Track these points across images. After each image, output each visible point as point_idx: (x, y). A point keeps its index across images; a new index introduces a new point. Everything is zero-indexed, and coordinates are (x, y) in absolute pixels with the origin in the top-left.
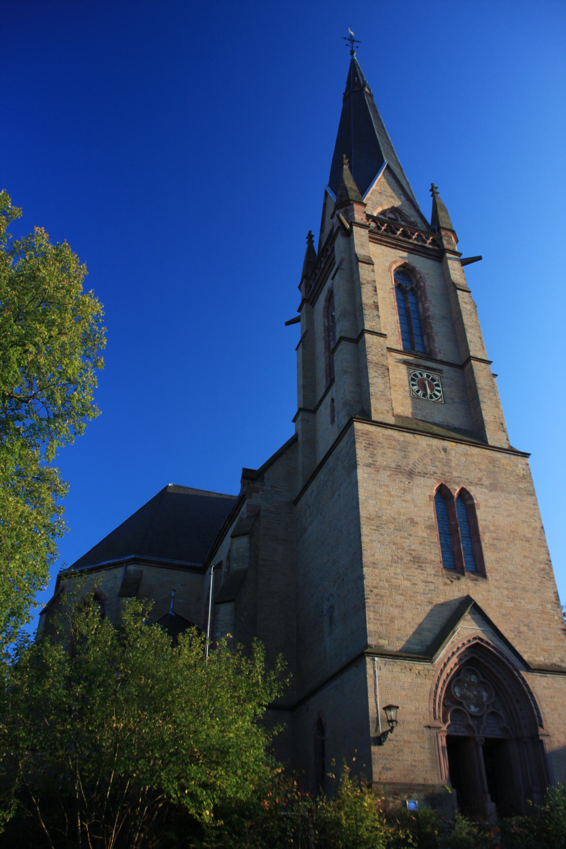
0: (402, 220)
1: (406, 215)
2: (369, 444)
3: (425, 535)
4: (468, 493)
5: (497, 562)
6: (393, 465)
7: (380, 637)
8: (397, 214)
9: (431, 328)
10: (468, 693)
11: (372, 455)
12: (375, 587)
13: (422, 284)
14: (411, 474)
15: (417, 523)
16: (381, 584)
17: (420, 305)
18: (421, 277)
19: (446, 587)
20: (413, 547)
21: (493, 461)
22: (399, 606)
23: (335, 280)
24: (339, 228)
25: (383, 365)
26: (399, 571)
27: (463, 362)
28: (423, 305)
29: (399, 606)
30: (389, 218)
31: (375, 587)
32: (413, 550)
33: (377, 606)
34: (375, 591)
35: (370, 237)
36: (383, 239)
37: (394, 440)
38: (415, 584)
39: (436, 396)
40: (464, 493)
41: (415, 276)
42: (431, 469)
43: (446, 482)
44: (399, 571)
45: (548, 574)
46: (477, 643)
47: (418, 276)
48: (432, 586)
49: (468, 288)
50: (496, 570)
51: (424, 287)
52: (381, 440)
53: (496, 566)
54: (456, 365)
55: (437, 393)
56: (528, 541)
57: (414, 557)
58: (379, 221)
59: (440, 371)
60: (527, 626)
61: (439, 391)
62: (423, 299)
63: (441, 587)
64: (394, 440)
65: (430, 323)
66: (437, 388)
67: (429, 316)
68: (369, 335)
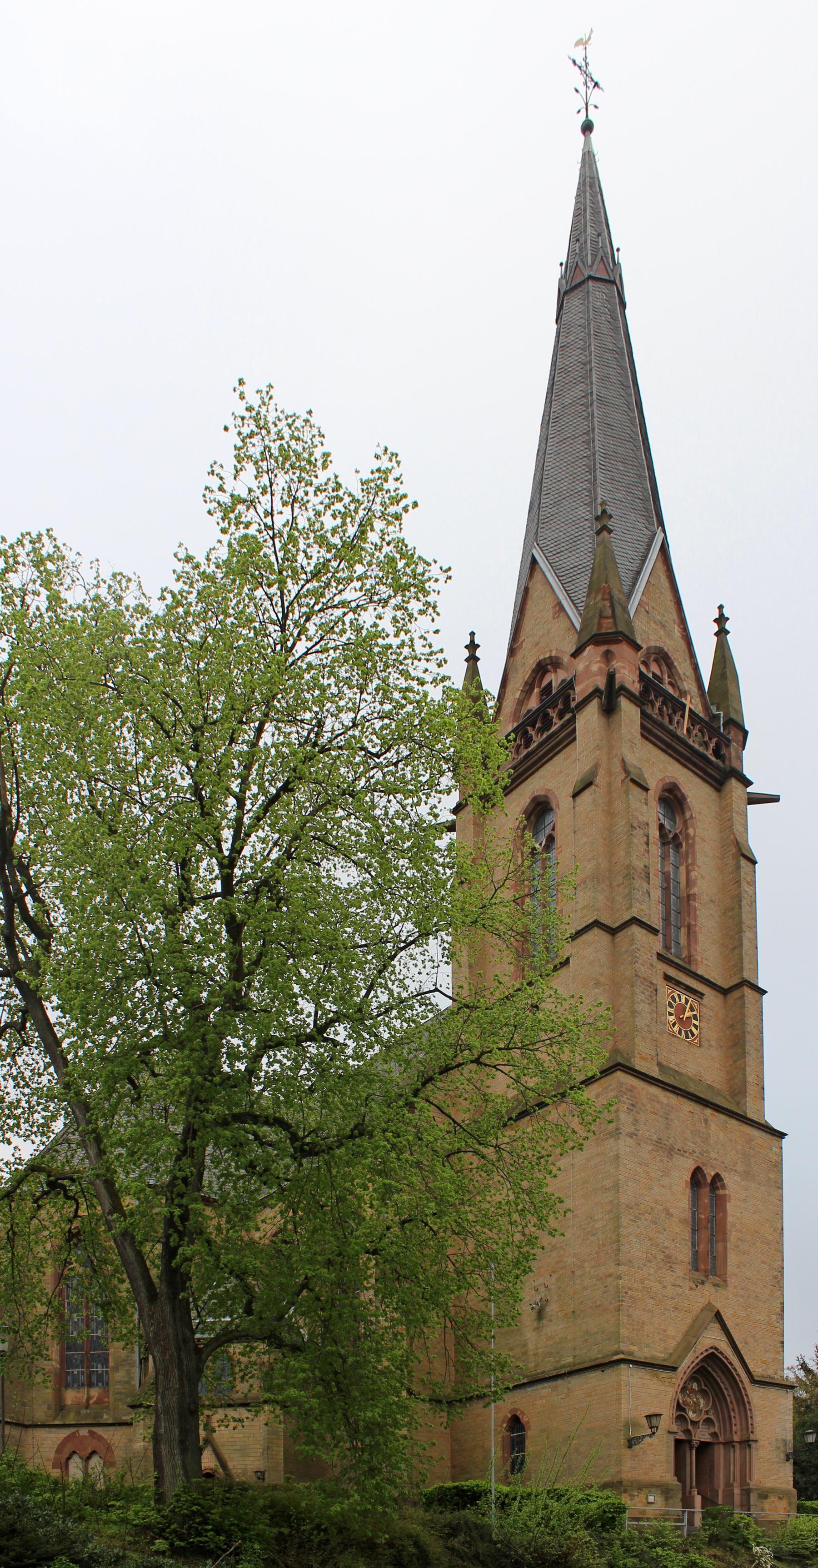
0: (670, 683)
1: (678, 672)
2: (632, 1105)
3: (678, 1230)
4: (721, 1180)
5: (738, 1266)
6: (655, 1137)
7: (632, 1344)
8: (665, 668)
9: (696, 918)
10: (689, 1400)
11: (636, 1122)
12: (630, 1289)
13: (691, 831)
14: (671, 1151)
15: (672, 1215)
16: (635, 1285)
17: (683, 869)
18: (691, 817)
19: (693, 1293)
20: (666, 1244)
21: (750, 1140)
22: (649, 1311)
23: (579, 799)
24: (596, 692)
25: (651, 983)
26: (652, 1271)
27: (617, 924)
28: (688, 873)
29: (649, 1311)
30: (654, 674)
31: (630, 1289)
32: (666, 1248)
33: (631, 1310)
34: (630, 1292)
35: (643, 727)
36: (655, 731)
37: (658, 1102)
38: (664, 1287)
39: (693, 1035)
40: (717, 1177)
41: (683, 813)
42: (690, 1146)
43: (704, 1164)
44: (652, 1271)
45: (778, 1282)
46: (713, 1353)
47: (688, 815)
48: (679, 1290)
49: (645, 780)
50: (736, 1275)
51: (693, 838)
52: (645, 1101)
53: (737, 1271)
54: (720, 987)
55: (693, 1029)
56: (768, 1244)
57: (666, 1256)
58: (655, 690)
59: (701, 995)
60: (753, 1337)
61: (696, 1027)
62: (690, 861)
63: (687, 1292)
64: (658, 1102)
65: (695, 909)
66: (694, 1022)
67: (694, 894)
68: (750, 991)
